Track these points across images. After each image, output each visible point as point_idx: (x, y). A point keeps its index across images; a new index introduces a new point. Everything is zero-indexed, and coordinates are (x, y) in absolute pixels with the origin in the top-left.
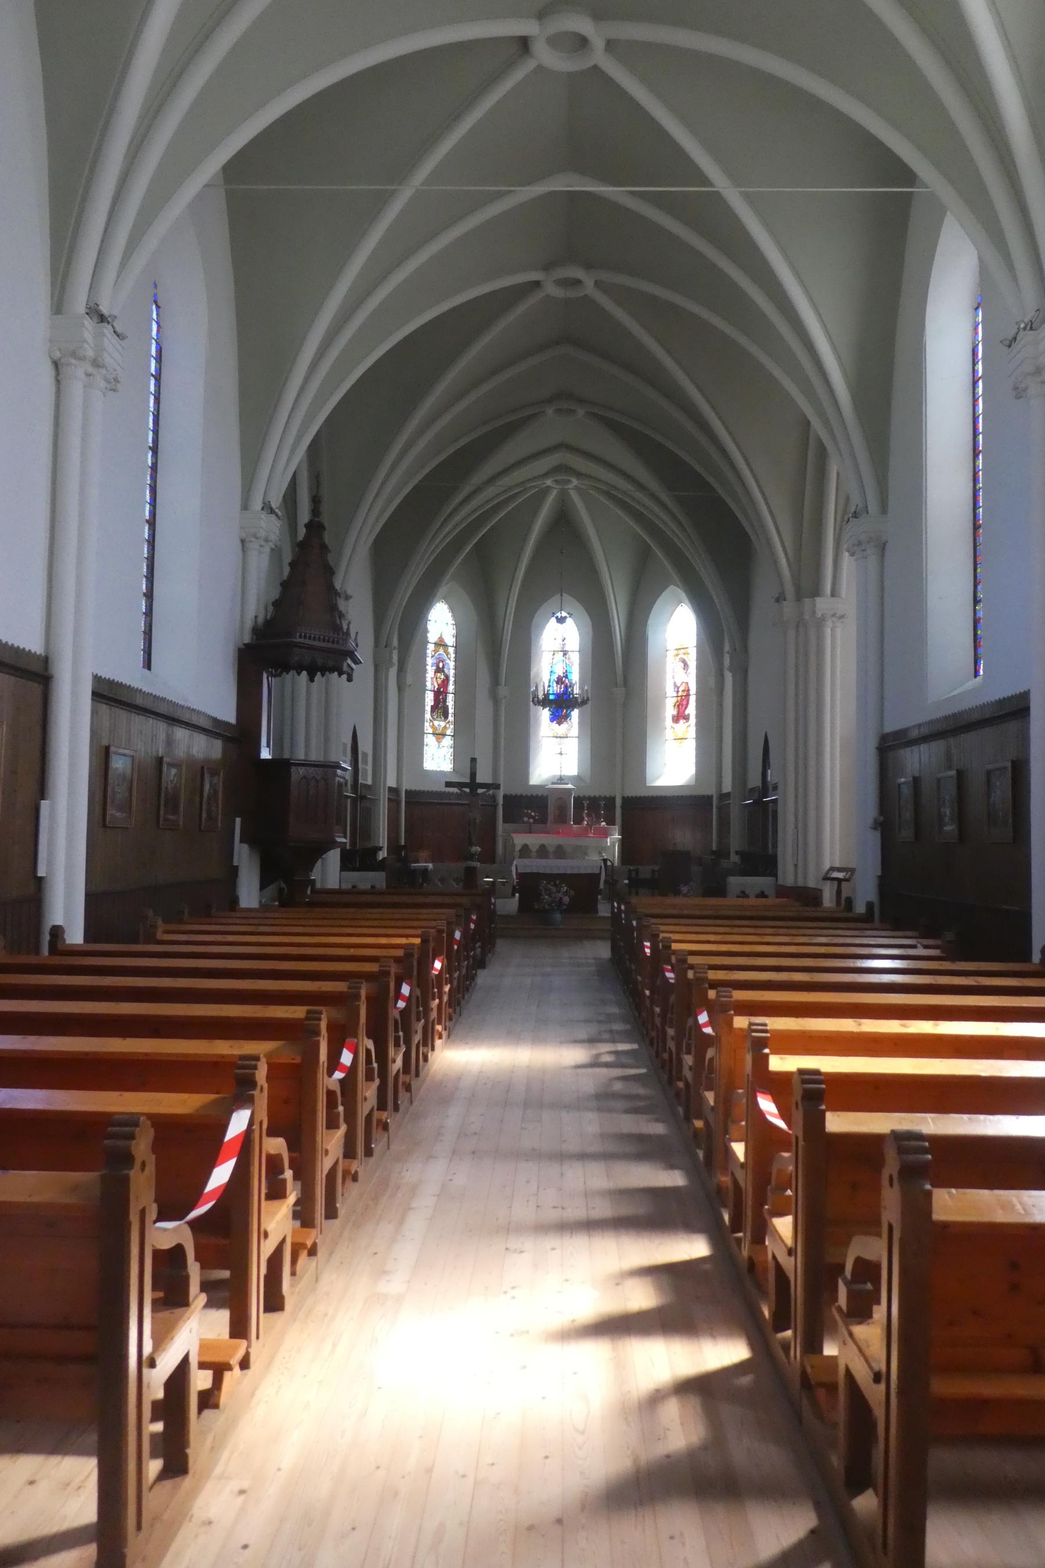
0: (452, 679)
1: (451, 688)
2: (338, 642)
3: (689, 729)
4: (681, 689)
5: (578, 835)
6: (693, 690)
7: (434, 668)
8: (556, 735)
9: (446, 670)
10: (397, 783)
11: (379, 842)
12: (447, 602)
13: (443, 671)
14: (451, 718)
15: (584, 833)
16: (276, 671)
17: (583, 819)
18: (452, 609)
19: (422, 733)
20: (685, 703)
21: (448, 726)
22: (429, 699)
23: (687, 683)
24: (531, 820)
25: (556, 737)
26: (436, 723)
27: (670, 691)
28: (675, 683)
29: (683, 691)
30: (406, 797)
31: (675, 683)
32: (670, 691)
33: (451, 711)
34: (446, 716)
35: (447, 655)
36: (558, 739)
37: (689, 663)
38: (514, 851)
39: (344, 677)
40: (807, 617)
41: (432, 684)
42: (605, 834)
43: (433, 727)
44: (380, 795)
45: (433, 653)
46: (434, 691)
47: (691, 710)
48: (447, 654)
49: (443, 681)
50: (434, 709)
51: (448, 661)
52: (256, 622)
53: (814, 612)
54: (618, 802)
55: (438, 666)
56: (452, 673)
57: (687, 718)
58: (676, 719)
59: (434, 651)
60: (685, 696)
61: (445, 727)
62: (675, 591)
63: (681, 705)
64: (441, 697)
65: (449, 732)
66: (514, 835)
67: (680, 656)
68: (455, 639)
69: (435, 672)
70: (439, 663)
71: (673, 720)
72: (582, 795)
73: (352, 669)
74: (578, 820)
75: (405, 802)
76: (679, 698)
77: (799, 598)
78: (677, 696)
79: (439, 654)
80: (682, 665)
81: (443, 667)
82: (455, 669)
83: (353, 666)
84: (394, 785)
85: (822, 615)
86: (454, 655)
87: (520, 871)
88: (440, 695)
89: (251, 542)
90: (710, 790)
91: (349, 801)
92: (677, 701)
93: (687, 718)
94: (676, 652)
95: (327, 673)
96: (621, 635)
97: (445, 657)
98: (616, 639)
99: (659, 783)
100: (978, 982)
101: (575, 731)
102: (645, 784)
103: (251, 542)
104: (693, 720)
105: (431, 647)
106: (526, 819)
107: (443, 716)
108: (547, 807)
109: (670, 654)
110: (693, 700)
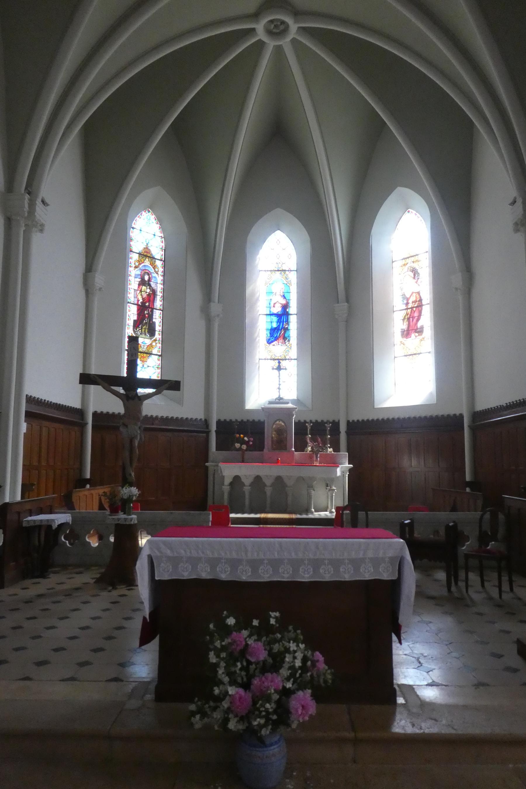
0: (159, 294)
1: (158, 303)
4: (410, 301)
5: (301, 464)
6: (427, 297)
8: (273, 357)
12: (154, 212)
13: (150, 285)
14: (158, 336)
15: (308, 462)
17: (306, 445)
18: (160, 220)
20: (416, 314)
21: (154, 344)
23: (419, 293)
24: (244, 447)
27: (398, 304)
29: (413, 302)
32: (398, 304)
33: (158, 328)
35: (154, 268)
38: (223, 484)
41: (136, 297)
42: (334, 463)
45: (137, 264)
46: (137, 305)
48: (154, 267)
49: (149, 295)
51: (155, 275)
54: (343, 428)
55: (143, 279)
56: (159, 288)
58: (406, 334)
59: (138, 261)
60: (416, 307)
64: (146, 312)
65: (155, 351)
66: (221, 465)
67: (408, 265)
69: (139, 285)
74: (301, 446)
75: (93, 425)
76: (409, 311)
78: (407, 309)
79: (145, 266)
80: (412, 274)
81: (149, 280)
82: (164, 284)
86: (163, 270)
87: (162, 575)
92: (407, 314)
93: (420, 331)
94: (404, 262)
97: (151, 270)
98: (338, 258)
99: (387, 404)
101: (293, 353)
102: (374, 406)
105: (134, 257)
106: (237, 445)
107: (149, 332)
108: (264, 433)
109: (397, 266)
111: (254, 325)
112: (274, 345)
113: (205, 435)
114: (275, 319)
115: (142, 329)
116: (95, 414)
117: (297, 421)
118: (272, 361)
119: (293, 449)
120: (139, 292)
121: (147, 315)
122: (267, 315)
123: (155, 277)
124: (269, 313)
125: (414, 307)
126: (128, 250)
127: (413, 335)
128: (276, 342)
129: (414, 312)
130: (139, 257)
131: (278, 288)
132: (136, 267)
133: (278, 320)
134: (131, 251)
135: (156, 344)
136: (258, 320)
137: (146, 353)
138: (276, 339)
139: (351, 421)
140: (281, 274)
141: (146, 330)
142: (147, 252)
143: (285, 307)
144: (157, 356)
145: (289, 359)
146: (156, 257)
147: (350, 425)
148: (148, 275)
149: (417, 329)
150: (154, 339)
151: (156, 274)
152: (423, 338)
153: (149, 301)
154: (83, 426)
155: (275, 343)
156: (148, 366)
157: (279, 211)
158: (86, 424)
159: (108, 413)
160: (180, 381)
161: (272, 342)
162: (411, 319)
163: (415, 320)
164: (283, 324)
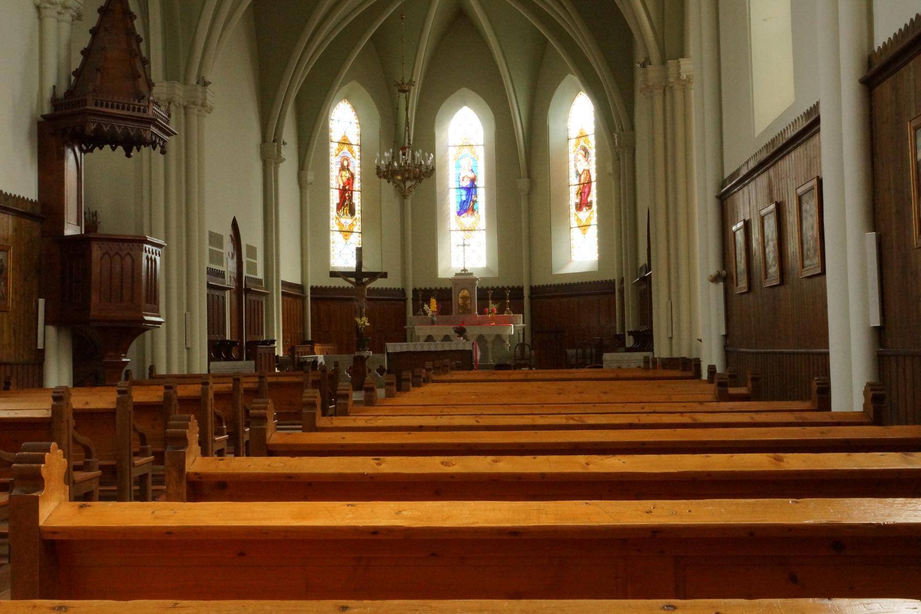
0: (357, 177)
1: (357, 185)
2: (139, 110)
3: (591, 216)
7: (339, 166)
9: (351, 168)
10: (302, 281)
11: (274, 336)
13: (348, 169)
14: (358, 215)
16: (87, 147)
18: (355, 108)
19: (326, 230)
20: (587, 190)
21: (355, 223)
22: (335, 197)
25: (464, 230)
26: (343, 220)
28: (577, 171)
30: (311, 294)
31: (577, 171)
32: (573, 180)
33: (358, 208)
34: (352, 212)
35: (352, 154)
36: (466, 232)
37: (589, 150)
39: (158, 148)
40: (671, 80)
43: (340, 224)
44: (273, 289)
45: (337, 152)
46: (339, 189)
47: (593, 197)
49: (348, 179)
50: (340, 206)
51: (352, 159)
52: (54, 93)
53: (679, 74)
54: (526, 293)
55: (342, 165)
57: (589, 205)
58: (579, 207)
61: (352, 225)
62: (572, 79)
63: (584, 192)
68: (359, 138)
69: (340, 171)
70: (343, 161)
71: (576, 208)
72: (485, 287)
73: (164, 141)
76: (581, 186)
77: (663, 62)
78: (580, 184)
80: (583, 153)
81: (348, 165)
83: (165, 137)
84: (297, 280)
85: (687, 76)
86: (359, 154)
88: (345, 193)
89: (46, 8)
90: (612, 275)
91: (228, 293)
92: (580, 189)
93: (589, 205)
95: (143, 147)
96: (522, 129)
97: (349, 155)
98: (518, 133)
100: (694, 419)
103: (46, 8)
104: (595, 207)
105: (334, 147)
107: (350, 213)
109: (572, 143)
110: (594, 186)
111: (445, 193)
112: (464, 217)
113: (402, 302)
114: (464, 192)
115: (344, 209)
116: (312, 288)
117: (480, 288)
118: (463, 232)
119: (477, 313)
120: (339, 177)
121: (347, 198)
122: (457, 188)
123: (353, 162)
124: (458, 187)
125: (585, 183)
126: (330, 141)
127: (584, 209)
128: (465, 214)
129: (585, 187)
130: (339, 145)
131: (466, 163)
132: (337, 155)
133: (467, 193)
134: (332, 141)
135: (356, 222)
136: (448, 193)
137: (348, 232)
138: (466, 211)
139: (533, 286)
140: (468, 148)
141: (348, 211)
142: (345, 140)
143: (473, 180)
144: (358, 234)
145: (478, 230)
146: (352, 143)
147: (533, 289)
148: (347, 160)
149: (588, 203)
150: (355, 217)
151: (353, 159)
152: (592, 212)
153: (349, 184)
154: (303, 298)
155: (465, 215)
156: (351, 243)
157: (464, 90)
158: (307, 297)
159: (339, 287)
160: (387, 277)
161: (462, 214)
162: (583, 194)
163: (586, 195)
164: (472, 197)
